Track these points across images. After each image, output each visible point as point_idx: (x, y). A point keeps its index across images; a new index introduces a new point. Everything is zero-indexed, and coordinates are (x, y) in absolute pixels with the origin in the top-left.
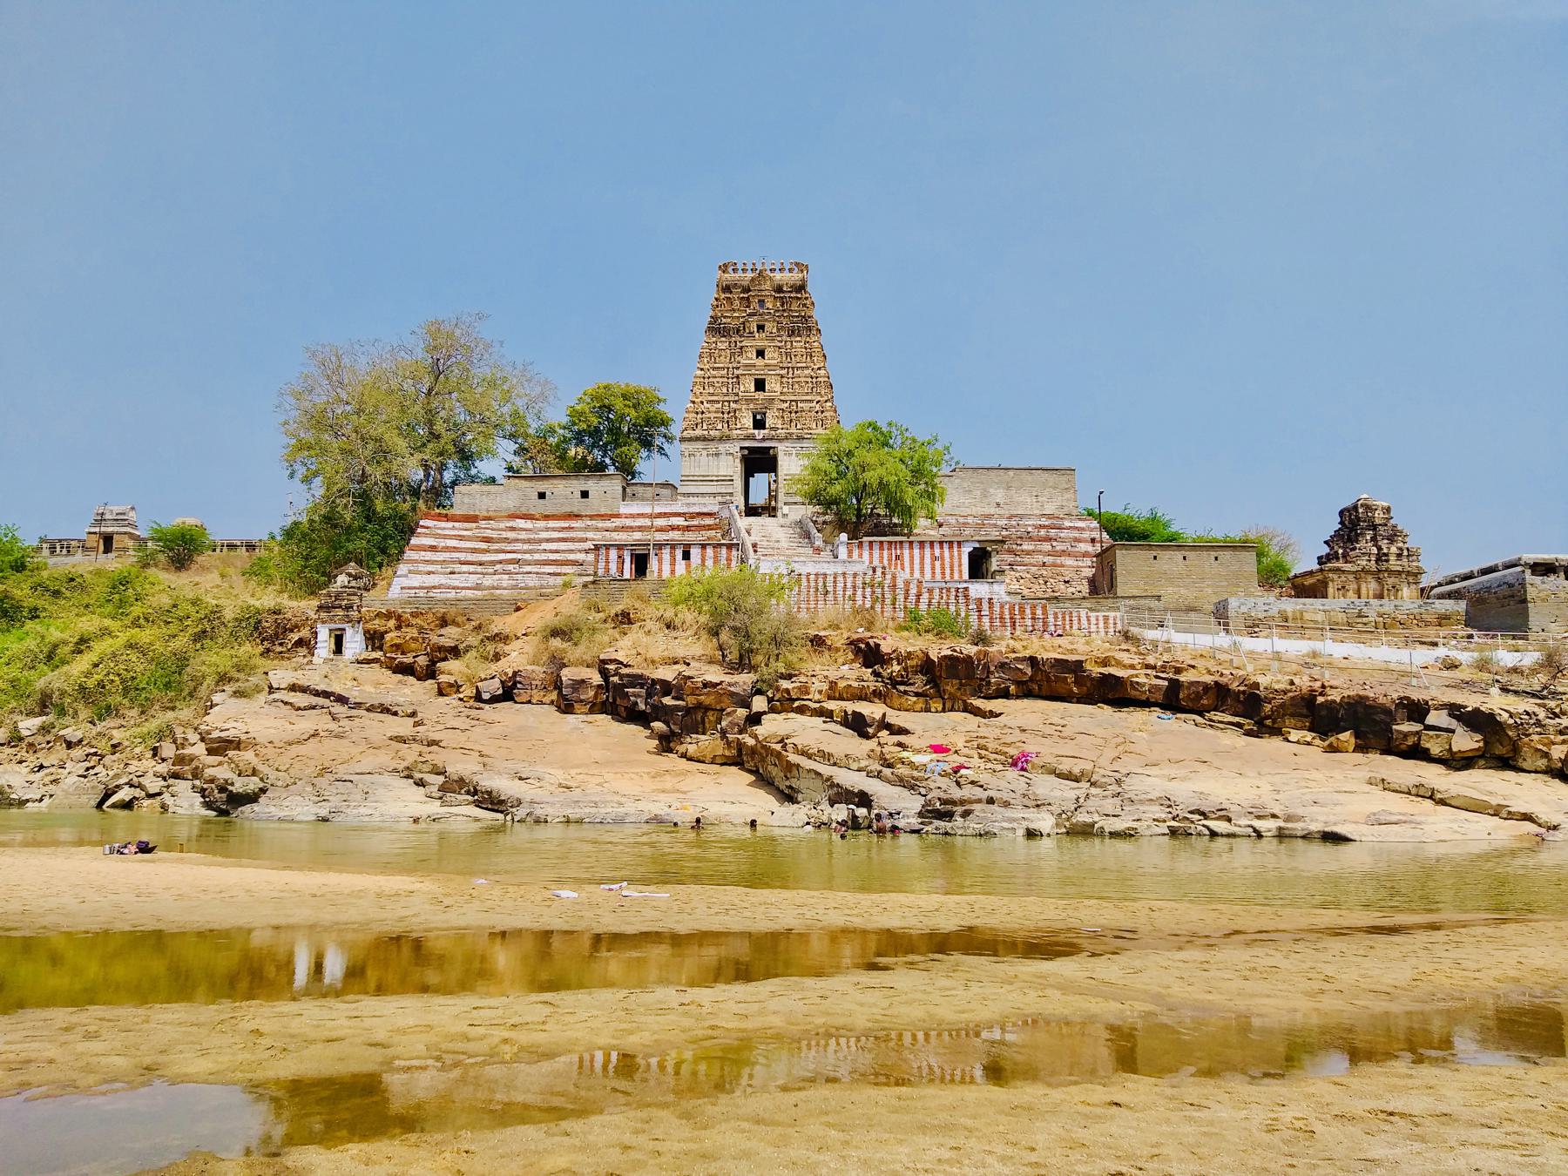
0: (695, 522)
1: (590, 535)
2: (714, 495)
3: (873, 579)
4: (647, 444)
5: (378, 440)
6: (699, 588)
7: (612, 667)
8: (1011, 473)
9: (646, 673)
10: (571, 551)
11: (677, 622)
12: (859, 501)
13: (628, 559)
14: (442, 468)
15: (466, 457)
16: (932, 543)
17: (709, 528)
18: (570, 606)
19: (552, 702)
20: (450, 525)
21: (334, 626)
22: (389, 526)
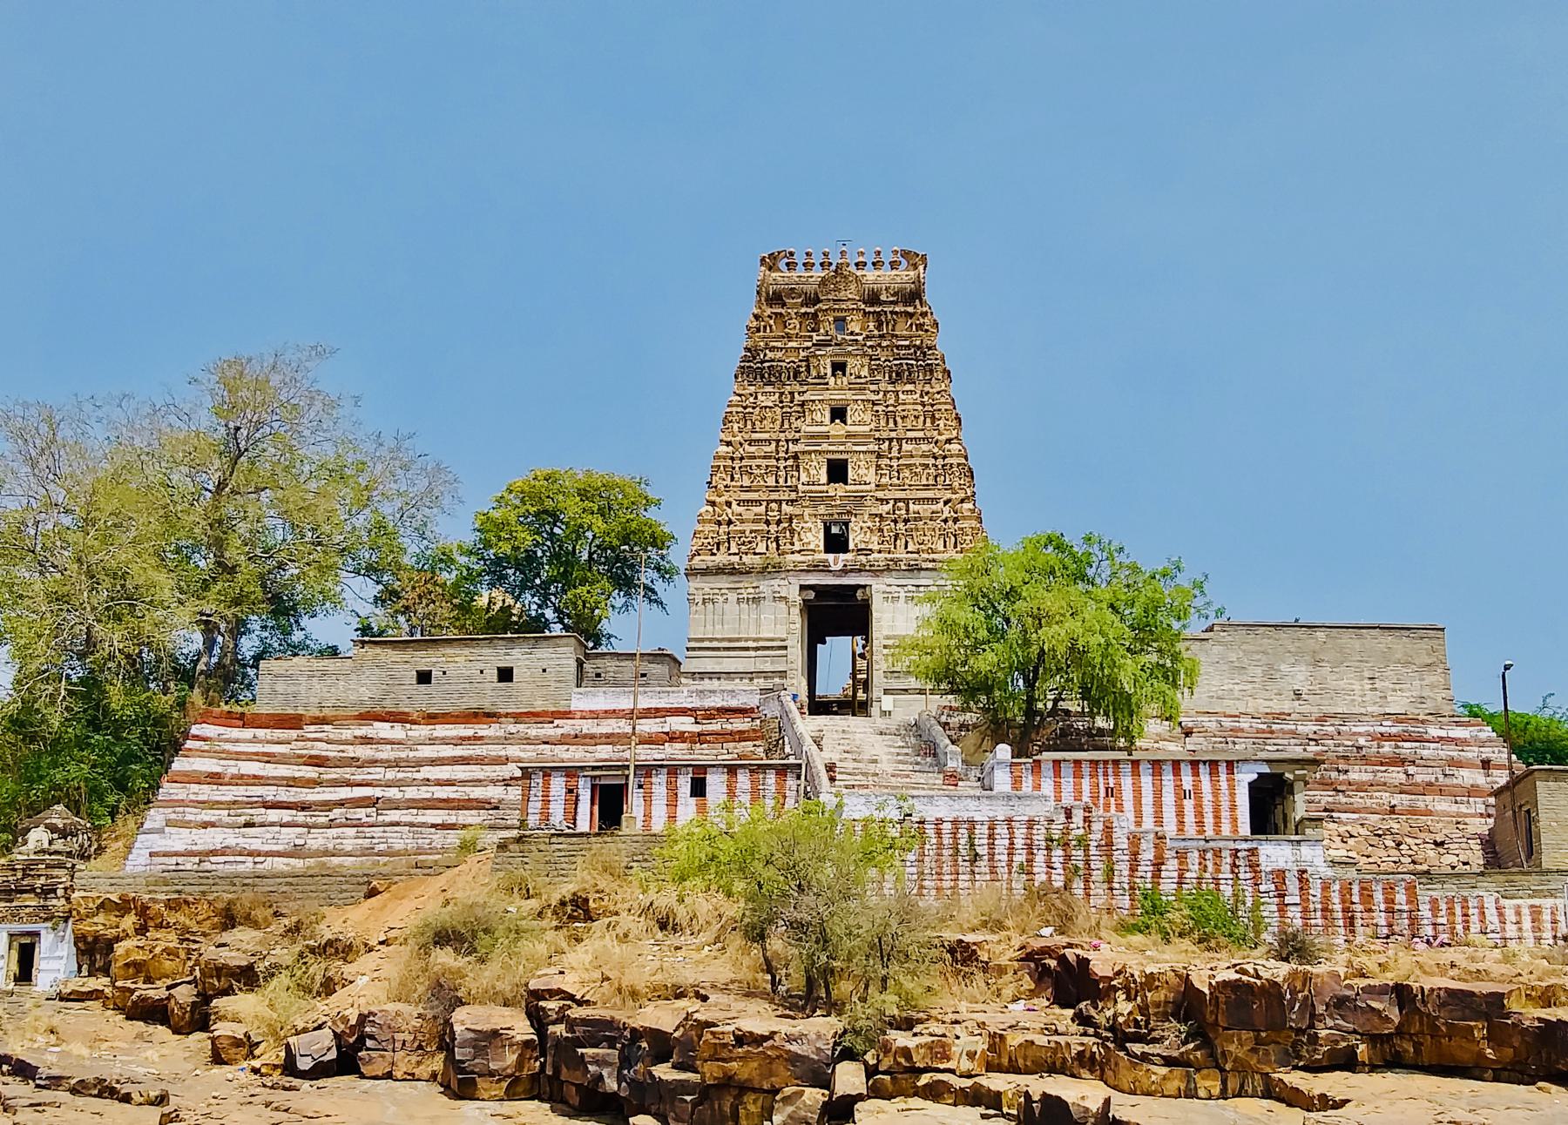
0: (715, 726)
1: (513, 751)
2: (751, 675)
3: (1066, 831)
4: (625, 582)
5: (119, 575)
6: (727, 845)
7: (552, 1005)
8: (1320, 635)
9: (621, 1016)
10: (477, 782)
11: (682, 914)
12: (1030, 684)
13: (585, 795)
14: (239, 629)
15: (283, 609)
16: (1176, 764)
17: (741, 736)
18: (472, 886)
19: (434, 1076)
20: (248, 733)
21: (17, 927)
22: (133, 736)
